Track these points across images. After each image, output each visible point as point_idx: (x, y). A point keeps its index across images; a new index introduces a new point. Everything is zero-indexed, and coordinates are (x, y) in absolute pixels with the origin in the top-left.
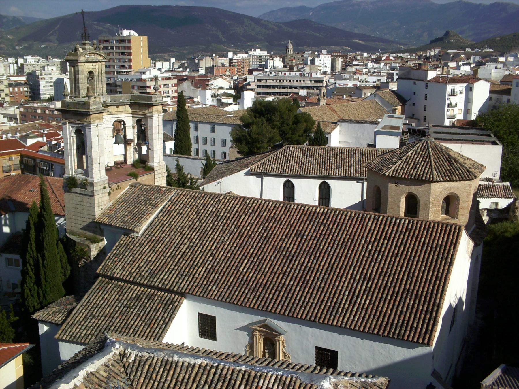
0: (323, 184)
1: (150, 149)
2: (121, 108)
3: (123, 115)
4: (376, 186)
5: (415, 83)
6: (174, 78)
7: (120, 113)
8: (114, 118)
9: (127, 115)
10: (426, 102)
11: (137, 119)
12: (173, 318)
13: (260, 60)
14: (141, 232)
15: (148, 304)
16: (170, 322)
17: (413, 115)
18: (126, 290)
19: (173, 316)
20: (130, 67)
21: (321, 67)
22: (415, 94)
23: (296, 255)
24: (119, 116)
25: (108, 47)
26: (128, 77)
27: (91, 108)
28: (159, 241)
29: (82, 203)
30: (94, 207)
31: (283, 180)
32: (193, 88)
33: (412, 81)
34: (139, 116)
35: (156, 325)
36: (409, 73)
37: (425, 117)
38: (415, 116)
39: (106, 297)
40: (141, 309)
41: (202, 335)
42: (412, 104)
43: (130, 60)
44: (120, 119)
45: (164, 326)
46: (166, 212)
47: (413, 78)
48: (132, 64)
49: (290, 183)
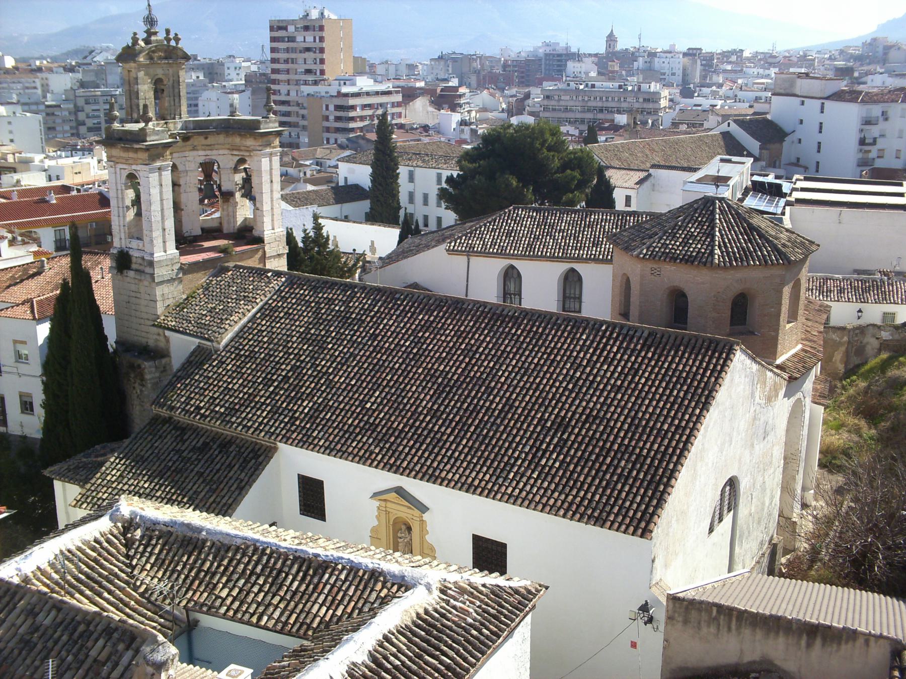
0: (510, 271)
1: (258, 209)
2: (211, 140)
3: (215, 152)
4: (624, 274)
5: (803, 103)
6: (397, 92)
7: (210, 147)
8: (200, 156)
9: (221, 152)
10: (820, 138)
11: (238, 158)
12: (254, 481)
13: (559, 61)
14: (224, 342)
15: (219, 458)
16: (247, 487)
17: (798, 159)
18: (189, 434)
19: (254, 477)
20: (322, 72)
21: (664, 74)
22: (801, 122)
23: (458, 384)
24: (208, 152)
25: (283, 38)
26: (321, 89)
27: (148, 139)
28: (252, 356)
29: (138, 295)
30: (155, 301)
31: (562, 268)
32: (431, 109)
33: (799, 100)
34: (241, 153)
35: (225, 491)
36: (792, 84)
37: (818, 163)
38: (801, 162)
39: (156, 445)
40: (207, 465)
41: (305, 510)
42: (796, 141)
43: (322, 61)
44: (213, 157)
45: (236, 493)
46: (267, 311)
47: (798, 93)
48: (324, 67)
49: (515, 271)
